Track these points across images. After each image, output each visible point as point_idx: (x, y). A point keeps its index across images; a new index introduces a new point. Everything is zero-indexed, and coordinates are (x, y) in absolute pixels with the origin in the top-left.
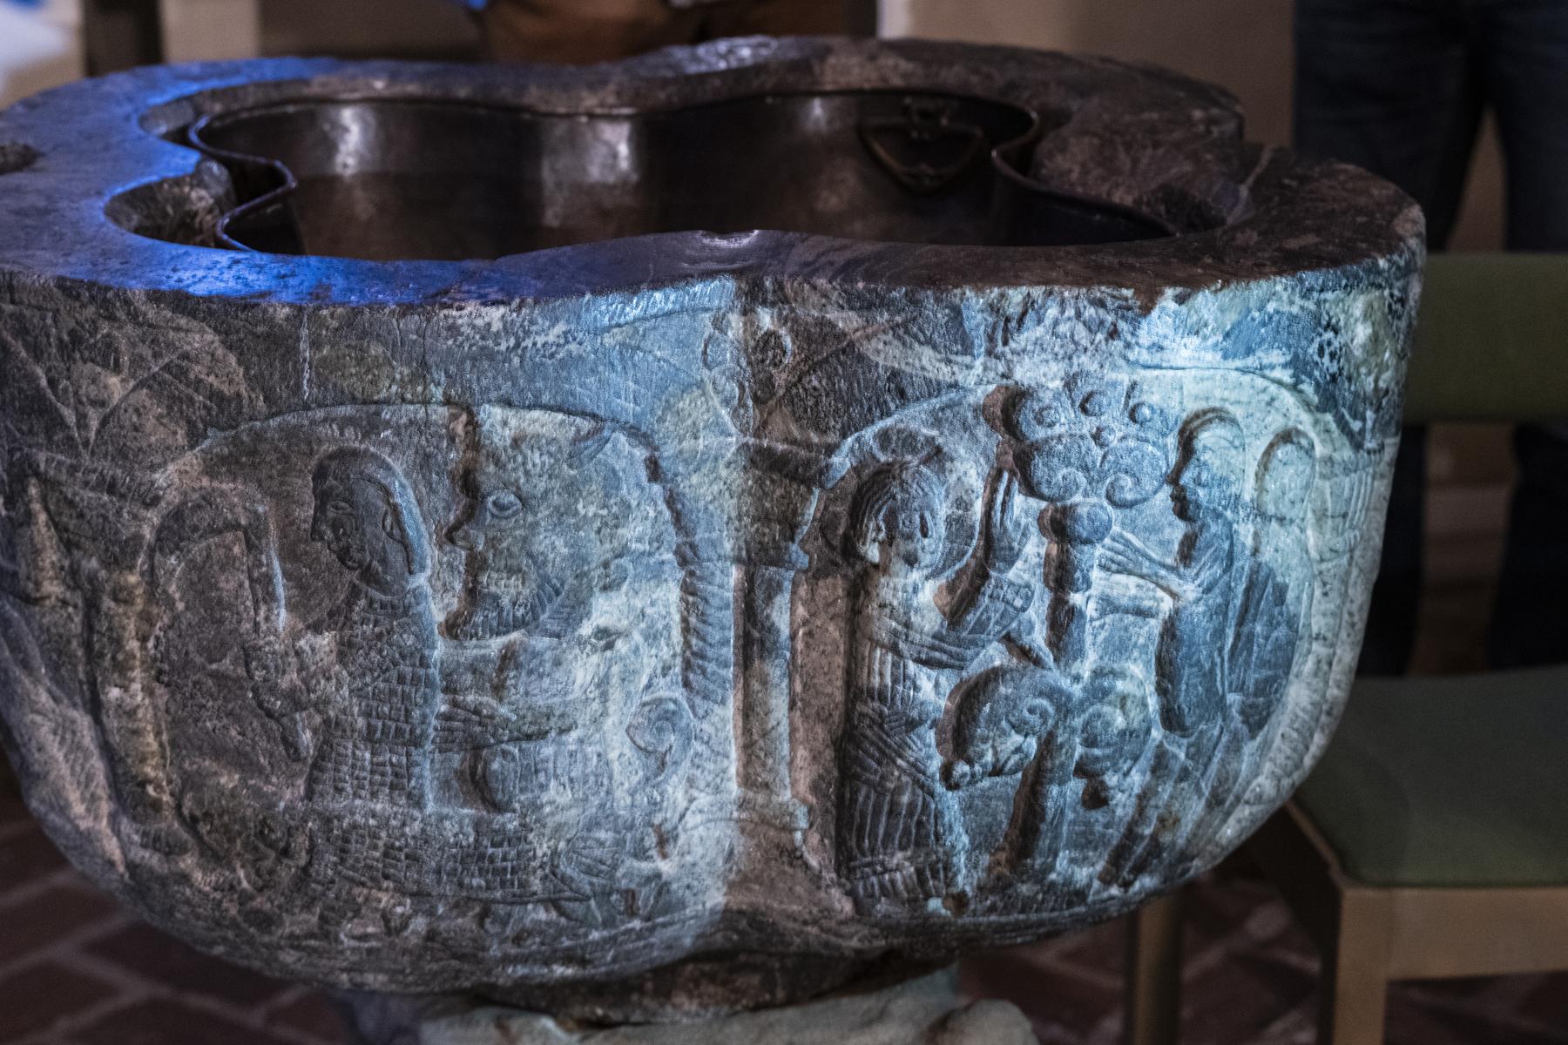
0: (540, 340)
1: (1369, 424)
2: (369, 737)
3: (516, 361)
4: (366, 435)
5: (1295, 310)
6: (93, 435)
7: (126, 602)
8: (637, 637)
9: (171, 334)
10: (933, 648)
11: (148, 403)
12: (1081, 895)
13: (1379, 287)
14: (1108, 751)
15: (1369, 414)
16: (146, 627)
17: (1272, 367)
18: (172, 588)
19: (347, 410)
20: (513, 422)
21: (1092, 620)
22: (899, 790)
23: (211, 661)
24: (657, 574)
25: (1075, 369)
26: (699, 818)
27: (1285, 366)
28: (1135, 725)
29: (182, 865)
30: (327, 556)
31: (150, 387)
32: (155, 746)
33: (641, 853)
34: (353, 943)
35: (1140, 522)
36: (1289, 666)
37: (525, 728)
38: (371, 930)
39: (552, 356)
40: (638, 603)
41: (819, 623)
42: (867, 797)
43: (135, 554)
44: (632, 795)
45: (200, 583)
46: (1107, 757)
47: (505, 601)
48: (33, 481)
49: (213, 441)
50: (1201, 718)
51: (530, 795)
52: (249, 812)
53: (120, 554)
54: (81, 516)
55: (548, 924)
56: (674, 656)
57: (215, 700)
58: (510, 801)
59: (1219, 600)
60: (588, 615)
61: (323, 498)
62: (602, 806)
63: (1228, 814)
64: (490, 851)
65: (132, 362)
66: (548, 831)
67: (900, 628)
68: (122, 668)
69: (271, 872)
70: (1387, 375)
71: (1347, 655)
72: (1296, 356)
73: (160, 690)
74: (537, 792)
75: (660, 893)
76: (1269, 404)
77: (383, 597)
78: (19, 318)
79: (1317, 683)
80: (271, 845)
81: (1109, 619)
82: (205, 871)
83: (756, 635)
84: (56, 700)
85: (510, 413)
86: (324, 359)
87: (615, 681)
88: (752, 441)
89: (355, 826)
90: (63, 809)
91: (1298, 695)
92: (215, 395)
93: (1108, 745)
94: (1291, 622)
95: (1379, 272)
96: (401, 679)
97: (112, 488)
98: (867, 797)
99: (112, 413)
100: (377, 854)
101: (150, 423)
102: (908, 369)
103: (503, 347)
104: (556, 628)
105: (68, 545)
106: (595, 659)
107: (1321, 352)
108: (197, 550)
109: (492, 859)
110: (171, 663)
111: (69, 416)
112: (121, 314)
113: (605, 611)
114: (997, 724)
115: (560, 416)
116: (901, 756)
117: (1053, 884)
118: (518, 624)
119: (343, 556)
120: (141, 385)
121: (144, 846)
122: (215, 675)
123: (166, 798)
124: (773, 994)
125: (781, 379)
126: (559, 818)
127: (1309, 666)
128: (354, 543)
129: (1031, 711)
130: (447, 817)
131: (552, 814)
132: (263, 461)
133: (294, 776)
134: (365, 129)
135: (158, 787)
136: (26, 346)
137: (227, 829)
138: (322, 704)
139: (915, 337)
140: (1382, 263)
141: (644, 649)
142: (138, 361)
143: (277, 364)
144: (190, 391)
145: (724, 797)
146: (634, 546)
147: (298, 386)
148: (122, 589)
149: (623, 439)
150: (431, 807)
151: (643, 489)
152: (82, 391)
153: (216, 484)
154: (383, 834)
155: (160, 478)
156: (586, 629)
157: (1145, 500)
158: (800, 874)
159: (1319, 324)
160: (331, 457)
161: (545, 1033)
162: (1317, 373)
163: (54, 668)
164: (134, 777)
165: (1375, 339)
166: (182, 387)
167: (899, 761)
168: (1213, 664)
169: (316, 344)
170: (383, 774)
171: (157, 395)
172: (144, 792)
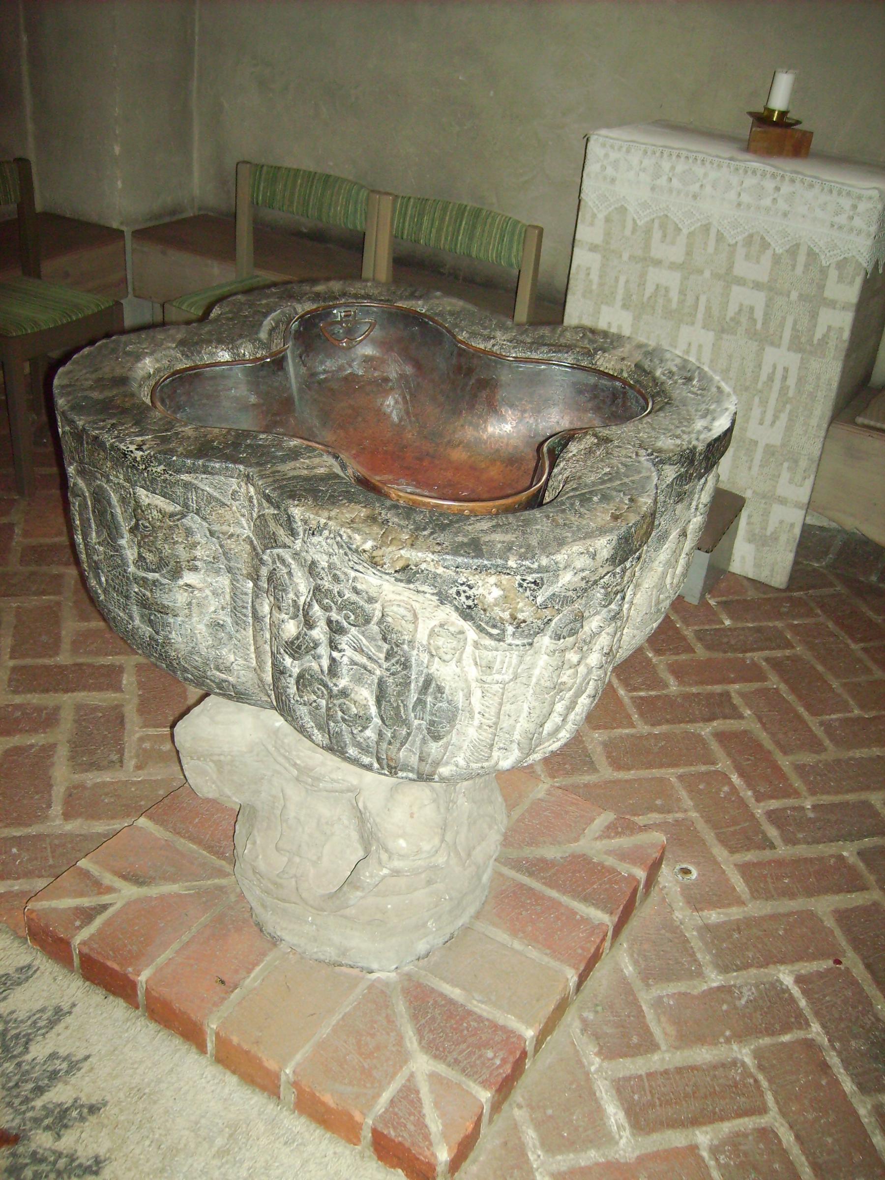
27: (433, 594)
81: (355, 667)
107: (458, 593)
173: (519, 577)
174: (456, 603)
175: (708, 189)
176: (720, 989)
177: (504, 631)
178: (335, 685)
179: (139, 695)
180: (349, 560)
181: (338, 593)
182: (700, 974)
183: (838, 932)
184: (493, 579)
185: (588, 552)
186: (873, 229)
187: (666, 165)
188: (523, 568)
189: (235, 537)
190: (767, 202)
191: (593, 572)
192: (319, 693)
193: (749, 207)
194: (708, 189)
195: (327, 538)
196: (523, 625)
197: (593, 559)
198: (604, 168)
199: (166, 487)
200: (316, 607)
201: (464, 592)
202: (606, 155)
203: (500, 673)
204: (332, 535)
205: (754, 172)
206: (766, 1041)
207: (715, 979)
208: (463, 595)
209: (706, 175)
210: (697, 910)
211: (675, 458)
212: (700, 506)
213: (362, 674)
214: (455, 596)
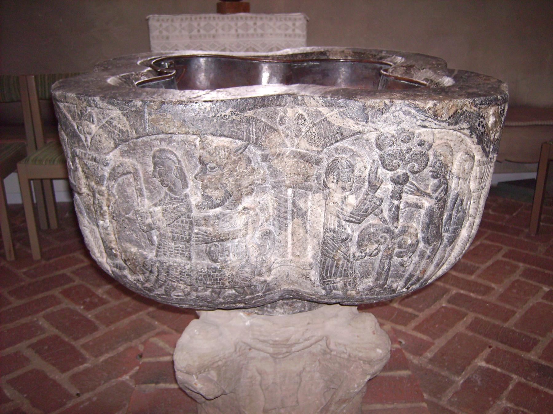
0: (223, 114)
1: (491, 149)
2: (173, 239)
3: (215, 120)
4: (168, 144)
5: (472, 110)
6: (89, 144)
7: (102, 195)
8: (258, 210)
9: (108, 111)
10: (350, 217)
11: (102, 133)
12: (394, 291)
13: (498, 105)
15: (492, 147)
16: (109, 203)
17: (463, 129)
18: (114, 192)
20: (215, 141)
22: (339, 260)
23: (127, 214)
24: (264, 191)
26: (278, 265)
27: (468, 129)
28: (414, 242)
29: (124, 273)
30: (158, 183)
31: (102, 128)
32: (114, 238)
33: (260, 275)
34: (175, 297)
36: (462, 225)
37: (221, 238)
38: (180, 294)
39: (227, 119)
40: (258, 200)
41: (315, 207)
42: (329, 262)
43: (103, 181)
44: (256, 258)
45: (122, 191)
46: (404, 252)
47: (214, 198)
48: (77, 158)
49: (123, 147)
50: (434, 241)
51: (224, 258)
52: (140, 259)
53: (99, 182)
54: (89, 168)
55: (232, 294)
56: (270, 216)
57: (128, 226)
58: (217, 260)
59: (442, 204)
60: (241, 203)
61: (155, 164)
62: (247, 261)
63: (440, 268)
64: (212, 274)
65: (98, 120)
66: (230, 269)
67: (340, 210)
68: (102, 215)
69: (148, 277)
70: (497, 134)
71: (478, 221)
72: (471, 126)
73: (114, 222)
74: (226, 257)
75: (267, 286)
76: (461, 142)
77: (175, 196)
78: (69, 107)
79: (470, 229)
80: (147, 269)
81: (407, 209)
82: (131, 275)
83: (295, 210)
84: (89, 223)
85: (214, 138)
86: (153, 119)
87: (250, 223)
88: (294, 149)
89: (170, 266)
90: (94, 254)
91: (464, 233)
92: (121, 131)
93: (405, 248)
94: (464, 211)
95: (498, 100)
96: (182, 222)
97: (95, 160)
98: (329, 262)
99: (93, 137)
100: (178, 274)
101: (103, 140)
102: (344, 126)
103: (210, 116)
104: (230, 207)
105: (87, 177)
106: (244, 217)
108: (120, 180)
109: (213, 276)
110: (116, 214)
111: (83, 139)
112: (93, 105)
113: (247, 202)
115: (231, 139)
116: (339, 250)
117: (386, 288)
118: (219, 205)
119: (162, 182)
120: (100, 128)
121: (114, 267)
122: (128, 218)
123: (118, 254)
124: (305, 309)
125: (304, 129)
126: (233, 265)
127: (467, 225)
128: (165, 179)
129: (381, 237)
130: (198, 264)
131: (231, 264)
132: (137, 152)
133: (152, 249)
135: (116, 250)
136: (71, 116)
137: (134, 264)
138: (158, 229)
139: (347, 116)
140: (499, 97)
141: (260, 214)
142: (99, 120)
143: (139, 120)
144: (113, 129)
145: (286, 259)
147: (145, 128)
148: (101, 191)
149: (252, 147)
150: (193, 261)
151: (259, 164)
152: (85, 130)
153: (124, 159)
154: (179, 268)
155: (108, 157)
156: (240, 207)
157: (421, 171)
158: (309, 282)
159: (479, 116)
160: (157, 151)
161: (241, 317)
162: (477, 132)
163: (88, 214)
164: (109, 247)
165: (495, 122)
166: (111, 128)
167: (339, 251)
168: (439, 224)
169: (150, 114)
170: (178, 250)
171: (104, 131)
172: (112, 252)
175: (220, 32)
176: (465, 382)
179: (26, 397)
180: (417, 120)
182: (451, 383)
183: (477, 336)
186: (305, 33)
187: (195, 24)
189: (281, 157)
190: (251, 31)
193: (243, 35)
194: (220, 32)
198: (161, 32)
200: (381, 171)
202: (161, 25)
205: (242, 18)
206: (506, 393)
207: (460, 380)
209: (217, 24)
210: (421, 355)
213: (412, 212)
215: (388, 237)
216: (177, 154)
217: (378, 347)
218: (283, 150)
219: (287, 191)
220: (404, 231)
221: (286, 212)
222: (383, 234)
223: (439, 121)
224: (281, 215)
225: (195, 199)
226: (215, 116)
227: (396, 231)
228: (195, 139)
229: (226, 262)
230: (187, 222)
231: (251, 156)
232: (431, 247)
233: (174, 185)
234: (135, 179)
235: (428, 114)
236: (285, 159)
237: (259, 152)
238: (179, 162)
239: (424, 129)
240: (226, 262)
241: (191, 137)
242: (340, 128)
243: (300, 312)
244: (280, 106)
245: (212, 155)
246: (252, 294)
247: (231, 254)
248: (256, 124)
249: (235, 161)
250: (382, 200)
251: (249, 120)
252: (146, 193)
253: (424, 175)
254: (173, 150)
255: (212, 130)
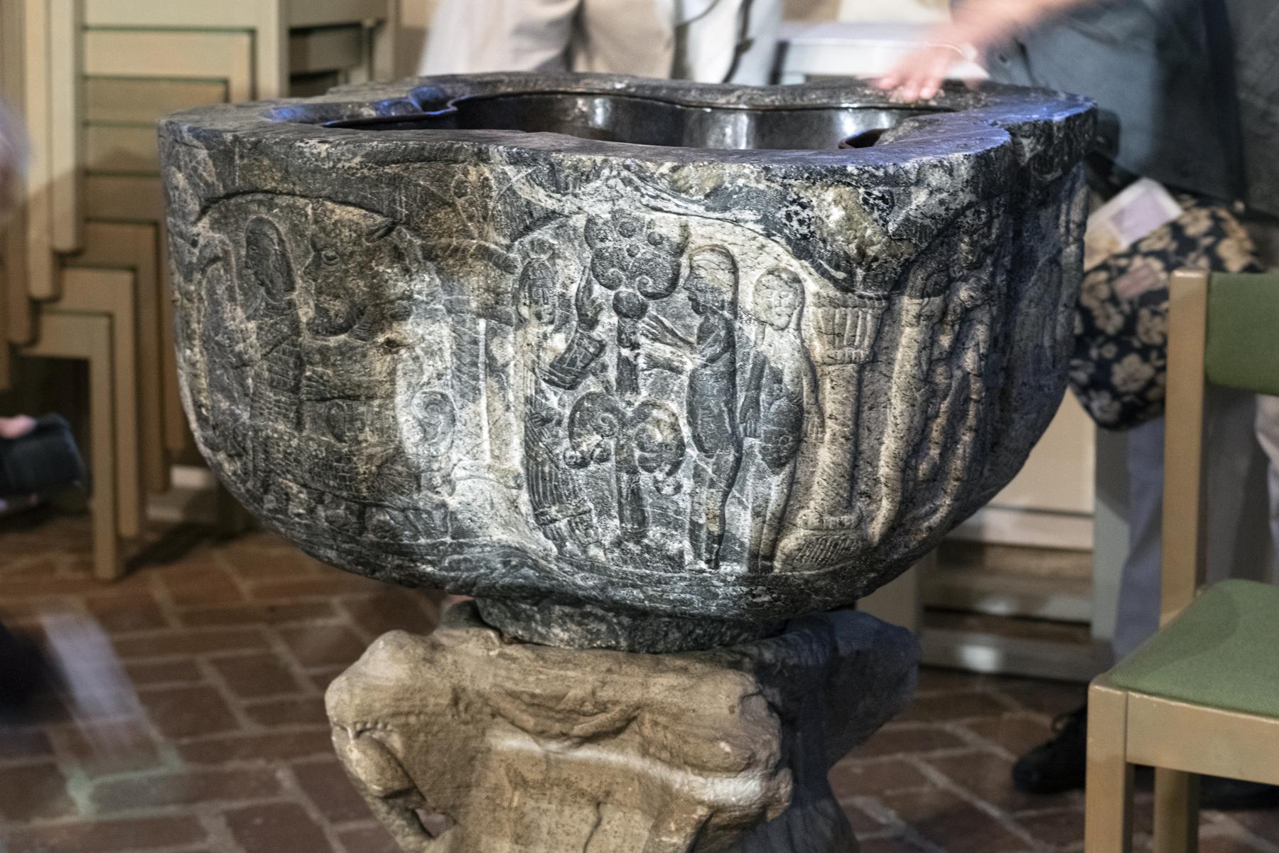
0: (347, 165)
14: (654, 455)
19: (260, 196)
20: (338, 211)
21: (643, 370)
25: (616, 208)
27: (757, 222)
35: (669, 311)
39: (353, 175)
47: (332, 313)
72: (765, 217)
81: (655, 371)
87: (400, 373)
89: (268, 437)
93: (652, 451)
107: (789, 217)
114: (584, 425)
126: (370, 450)
129: (603, 420)
130: (312, 439)
134: (606, 109)
146: (416, 296)
156: (381, 339)
169: (242, 157)
173: (862, 190)
174: (787, 231)
177: (852, 274)
178: (629, 404)
180: (643, 196)
181: (628, 250)
184: (830, 195)
185: (942, 166)
188: (866, 175)
189: (459, 254)
191: (954, 195)
192: (606, 427)
195: (607, 179)
196: (874, 265)
197: (951, 175)
199: (362, 189)
200: (598, 289)
201: (797, 213)
203: (851, 344)
204: (615, 173)
208: (795, 218)
211: (1026, 128)
212: (1072, 226)
213: (665, 379)
214: (784, 221)
215: (615, 421)
216: (281, 229)
217: (722, 739)
218: (466, 242)
219: (476, 324)
220: (642, 414)
221: (475, 364)
222: (606, 414)
223: (685, 200)
224: (464, 369)
225: (305, 313)
226: (334, 167)
227: (629, 412)
228: (307, 205)
229: (359, 443)
230: (291, 353)
231: (402, 246)
232: (713, 460)
233: (271, 281)
234: (226, 271)
235: (661, 186)
236: (470, 261)
237: (418, 242)
238: (281, 242)
239: (659, 214)
240: (359, 443)
241: (301, 202)
242: (528, 202)
243: (608, 648)
244: (456, 162)
245: (328, 235)
246: (429, 535)
247: (367, 429)
248: (406, 188)
249: (368, 249)
250: (601, 347)
251: (394, 181)
252: (239, 297)
253: (679, 305)
254: (275, 221)
255: (328, 191)
